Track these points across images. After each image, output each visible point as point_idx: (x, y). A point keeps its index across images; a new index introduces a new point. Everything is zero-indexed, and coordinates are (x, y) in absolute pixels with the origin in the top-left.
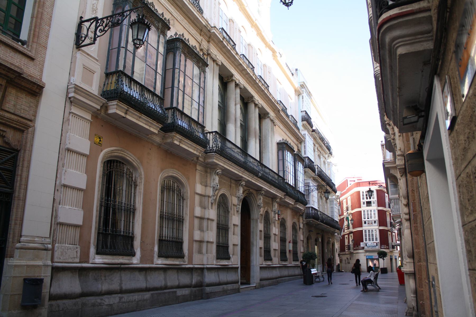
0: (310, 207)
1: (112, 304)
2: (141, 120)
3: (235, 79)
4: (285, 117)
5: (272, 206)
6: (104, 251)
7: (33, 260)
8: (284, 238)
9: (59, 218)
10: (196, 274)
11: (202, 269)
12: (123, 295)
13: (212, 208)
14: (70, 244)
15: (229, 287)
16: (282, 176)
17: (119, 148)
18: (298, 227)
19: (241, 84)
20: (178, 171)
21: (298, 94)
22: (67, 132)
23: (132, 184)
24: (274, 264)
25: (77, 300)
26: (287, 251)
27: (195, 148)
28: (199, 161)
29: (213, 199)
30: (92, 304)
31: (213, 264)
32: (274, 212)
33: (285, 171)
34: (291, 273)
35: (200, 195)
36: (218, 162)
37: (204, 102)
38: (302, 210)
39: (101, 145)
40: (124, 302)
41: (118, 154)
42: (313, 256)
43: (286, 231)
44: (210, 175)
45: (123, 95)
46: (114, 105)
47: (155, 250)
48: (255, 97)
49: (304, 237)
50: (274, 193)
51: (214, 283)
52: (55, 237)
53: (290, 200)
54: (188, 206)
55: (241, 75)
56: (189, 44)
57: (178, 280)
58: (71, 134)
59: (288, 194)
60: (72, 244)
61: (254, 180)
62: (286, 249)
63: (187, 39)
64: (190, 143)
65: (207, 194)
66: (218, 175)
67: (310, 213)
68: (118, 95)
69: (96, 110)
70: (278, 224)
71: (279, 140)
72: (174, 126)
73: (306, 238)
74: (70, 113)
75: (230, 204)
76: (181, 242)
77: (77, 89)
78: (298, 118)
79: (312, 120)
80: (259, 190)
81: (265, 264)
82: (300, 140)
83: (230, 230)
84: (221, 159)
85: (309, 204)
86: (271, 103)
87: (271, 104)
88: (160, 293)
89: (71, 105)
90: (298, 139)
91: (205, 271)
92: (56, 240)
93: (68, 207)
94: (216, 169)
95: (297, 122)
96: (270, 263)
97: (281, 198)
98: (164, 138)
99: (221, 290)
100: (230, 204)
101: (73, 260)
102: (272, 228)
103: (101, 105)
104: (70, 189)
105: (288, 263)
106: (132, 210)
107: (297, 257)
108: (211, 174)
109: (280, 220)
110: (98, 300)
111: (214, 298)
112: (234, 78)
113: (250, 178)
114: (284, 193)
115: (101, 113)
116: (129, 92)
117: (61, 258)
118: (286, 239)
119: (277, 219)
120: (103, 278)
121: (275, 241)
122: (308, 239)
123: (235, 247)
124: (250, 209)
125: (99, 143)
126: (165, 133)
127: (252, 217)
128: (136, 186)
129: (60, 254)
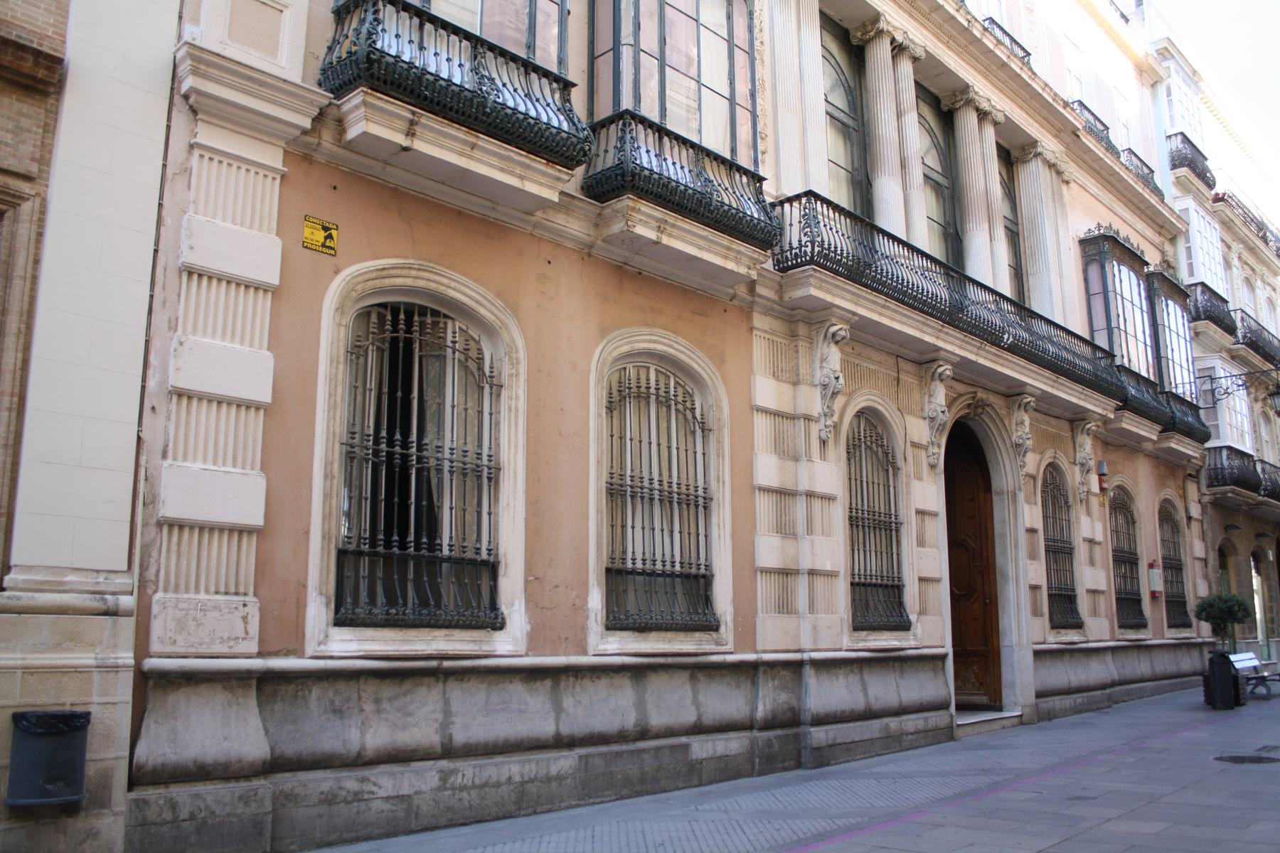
0: (1221, 448)
1: (409, 796)
2: (477, 154)
3: (891, 29)
4: (1099, 151)
5: (1071, 445)
6: (397, 614)
7: (57, 647)
9: (161, 502)
12: (458, 764)
13: (823, 457)
14: (217, 593)
15: (910, 723)
16: (1107, 348)
17: (412, 261)
18: (1181, 516)
19: (914, 43)
20: (672, 336)
21: (1151, 78)
23: (694, 428)
24: (1091, 639)
25: (255, 783)
26: (1142, 596)
27: (728, 249)
28: (757, 299)
29: (826, 426)
30: (323, 797)
31: (837, 646)
32: (1082, 465)
34: (1162, 668)
35: (776, 414)
36: (829, 298)
38: (1196, 458)
39: (333, 252)
40: (463, 788)
41: (409, 282)
42: (1236, 608)
44: (808, 345)
45: (380, 68)
46: (357, 107)
47: (590, 605)
48: (976, 89)
49: (1206, 547)
50: (1075, 400)
51: (843, 712)
52: (152, 570)
53: (1142, 426)
54: (723, 451)
55: (911, 16)
58: (201, 217)
59: (1127, 404)
60: (226, 593)
61: (985, 358)
62: (1139, 590)
64: (704, 233)
65: (802, 409)
66: (837, 343)
67: (1223, 468)
68: (360, 69)
69: (298, 133)
70: (1102, 505)
71: (1086, 230)
73: (1213, 550)
76: (704, 576)
77: (202, 59)
78: (1159, 161)
79: (1209, 164)
80: (1013, 393)
81: (1054, 640)
82: (1171, 232)
84: (841, 284)
85: (1218, 437)
86: (1043, 107)
87: (1044, 112)
88: (619, 754)
89: (196, 121)
90: (1162, 227)
91: (809, 672)
92: (157, 581)
93: (199, 465)
94: (828, 324)
95: (1152, 172)
97: (1106, 421)
98: (599, 222)
99: (878, 735)
100: (901, 441)
102: (1078, 518)
103: (315, 112)
104: (205, 403)
105: (1151, 636)
106: (701, 501)
109: (1112, 494)
110: (349, 781)
111: (848, 761)
112: (882, 25)
114: (1113, 403)
115: (319, 144)
116: (533, 113)
117: (180, 639)
119: (1095, 488)
121: (1092, 562)
122: (1223, 554)
123: (931, 588)
125: (324, 245)
126: (602, 203)
128: (497, 388)
129: (172, 625)
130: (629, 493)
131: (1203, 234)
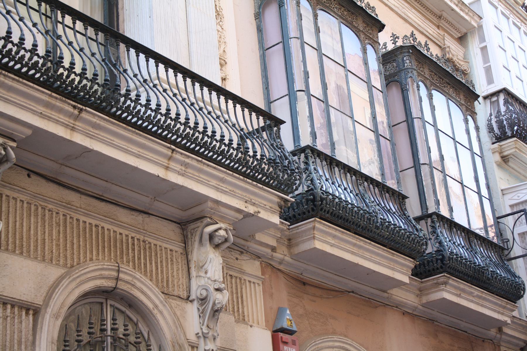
20: (345, 339)
28: (503, 337)
37: (488, 187)
56: (432, 55)
63: (423, 44)
66: (217, 246)
72: (314, 200)
98: (421, 292)
126: (421, 279)
131: (517, 43)
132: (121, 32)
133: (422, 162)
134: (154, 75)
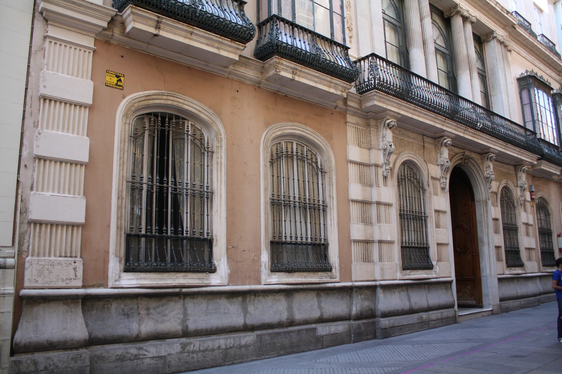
1: (165, 356)
2: (194, 37)
8: (548, 230)
10: (359, 297)
11: (373, 289)
12: (192, 340)
13: (385, 185)
14: (60, 256)
15: (434, 315)
16: (532, 130)
20: (304, 126)
22: (42, 69)
24: (528, 272)
26: (555, 250)
27: (331, 82)
28: (348, 108)
33: (537, 121)
36: (385, 106)
39: (121, 88)
41: (163, 102)
43: (551, 219)
44: (376, 130)
50: (516, 155)
51: (398, 310)
57: (320, 308)
61: (468, 135)
64: (317, 75)
65: (373, 162)
66: (390, 128)
70: (532, 206)
74: (45, 37)
75: (426, 176)
76: (426, 248)
80: (484, 152)
81: (509, 273)
83: (429, 220)
88: (278, 334)
91: (379, 291)
92: (28, 251)
94: (385, 119)
96: (520, 272)
97: (533, 166)
98: (263, 70)
100: (426, 176)
101: (67, 283)
102: (519, 213)
103: (109, 19)
104: (53, 163)
107: (428, 257)
108: (378, 129)
110: (132, 349)
113: (461, 132)
114: (536, 156)
115: (113, 35)
118: (550, 230)
120: (143, 312)
123: (443, 248)
124: (473, 184)
126: (264, 61)
127: (477, 198)
130: (283, 204)
132: (491, 110)
133: (535, 119)
134: (423, 85)
